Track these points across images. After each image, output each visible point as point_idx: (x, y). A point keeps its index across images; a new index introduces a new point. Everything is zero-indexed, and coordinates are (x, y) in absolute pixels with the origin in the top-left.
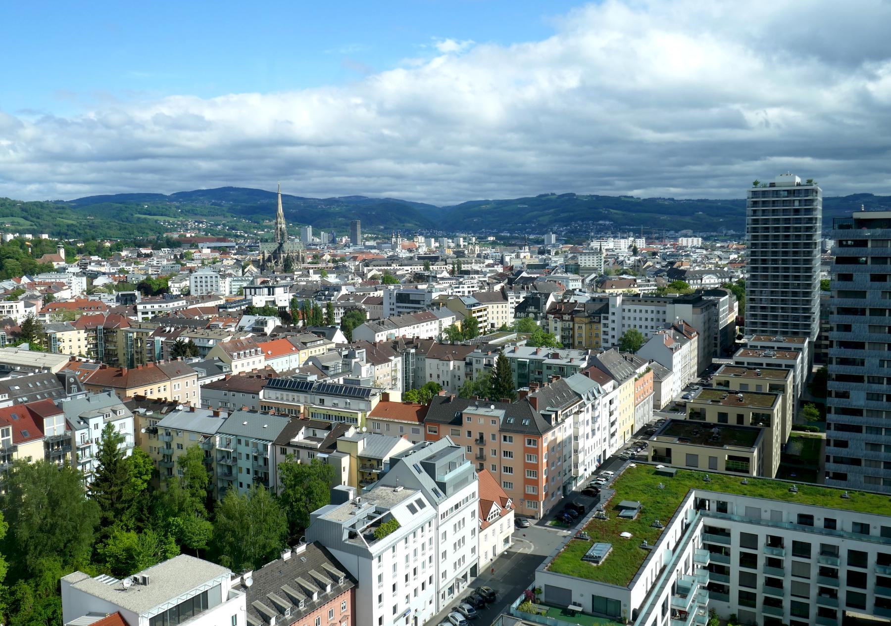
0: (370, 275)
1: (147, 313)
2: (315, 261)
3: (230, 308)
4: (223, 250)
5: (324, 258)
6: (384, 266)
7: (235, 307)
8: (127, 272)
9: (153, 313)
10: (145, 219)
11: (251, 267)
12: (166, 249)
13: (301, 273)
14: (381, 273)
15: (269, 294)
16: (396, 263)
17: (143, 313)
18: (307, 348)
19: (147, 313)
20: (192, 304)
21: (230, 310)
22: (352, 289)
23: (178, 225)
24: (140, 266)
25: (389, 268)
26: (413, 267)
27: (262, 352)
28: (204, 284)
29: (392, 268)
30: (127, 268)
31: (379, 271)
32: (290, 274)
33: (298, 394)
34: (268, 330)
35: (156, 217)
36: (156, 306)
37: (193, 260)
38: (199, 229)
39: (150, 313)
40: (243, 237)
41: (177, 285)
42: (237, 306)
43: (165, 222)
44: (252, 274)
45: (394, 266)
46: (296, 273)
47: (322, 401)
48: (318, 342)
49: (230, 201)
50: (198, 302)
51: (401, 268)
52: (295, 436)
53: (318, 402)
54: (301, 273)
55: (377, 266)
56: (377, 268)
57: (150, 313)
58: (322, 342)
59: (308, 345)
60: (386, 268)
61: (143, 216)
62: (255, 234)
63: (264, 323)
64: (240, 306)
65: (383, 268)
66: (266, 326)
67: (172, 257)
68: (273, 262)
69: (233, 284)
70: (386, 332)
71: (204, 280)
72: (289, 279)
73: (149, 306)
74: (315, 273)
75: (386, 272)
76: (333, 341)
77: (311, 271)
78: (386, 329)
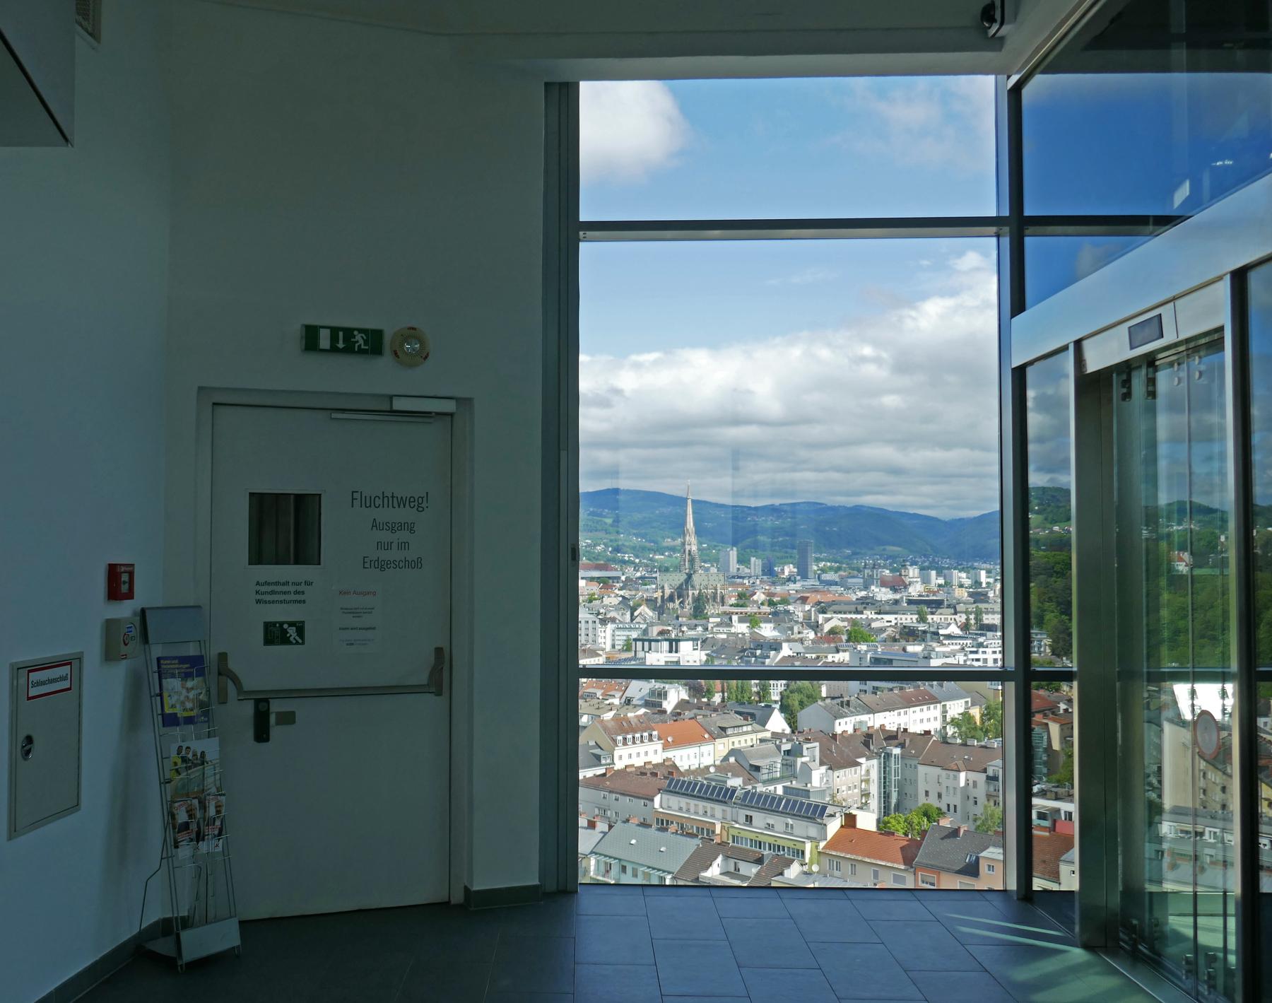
0: (827, 628)
2: (741, 602)
5: (755, 598)
6: (850, 613)
11: (644, 610)
13: (719, 620)
14: (846, 624)
15: (671, 651)
16: (871, 609)
18: (727, 736)
22: (799, 648)
25: (859, 616)
26: (899, 616)
27: (659, 739)
29: (864, 617)
31: (843, 620)
32: (703, 622)
33: (712, 805)
34: (669, 705)
40: (633, 563)
44: (645, 620)
45: (869, 614)
46: (711, 620)
47: (749, 819)
48: (745, 729)
51: (879, 617)
52: (707, 868)
53: (743, 819)
54: (719, 620)
55: (840, 612)
56: (840, 616)
58: (749, 728)
59: (729, 732)
60: (854, 616)
62: (651, 560)
63: (663, 695)
65: (849, 616)
66: (666, 699)
69: (617, 633)
70: (853, 719)
74: (741, 621)
75: (854, 623)
76: (767, 727)
77: (735, 618)
78: (853, 714)
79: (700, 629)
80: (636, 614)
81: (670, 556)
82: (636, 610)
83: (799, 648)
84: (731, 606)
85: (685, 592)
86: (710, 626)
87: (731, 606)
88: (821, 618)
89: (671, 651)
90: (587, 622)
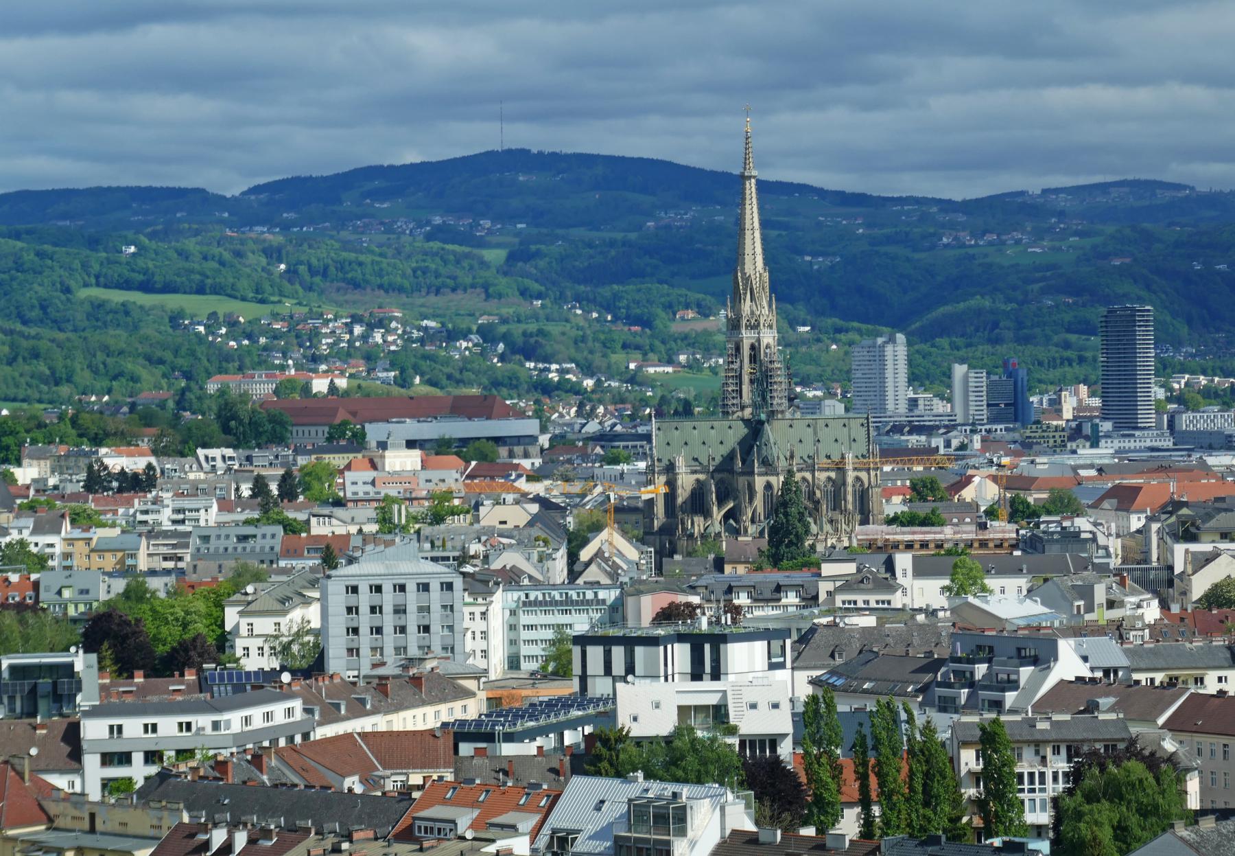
1: (124, 758)
2: (923, 509)
3: (510, 738)
4: (482, 457)
5: (968, 494)
7: (531, 735)
8: (41, 562)
9: (152, 757)
10: (125, 309)
12: (215, 452)
15: (696, 675)
17: (108, 759)
19: (124, 758)
20: (331, 716)
21: (508, 749)
23: (276, 336)
24: (98, 534)
28: (388, 621)
30: (39, 542)
35: (173, 301)
36: (168, 725)
37: (339, 503)
38: (370, 358)
39: (138, 758)
40: (576, 390)
41: (265, 625)
42: (543, 731)
43: (213, 321)
44: (614, 573)
46: (827, 569)
49: (514, 217)
50: (358, 710)
54: (851, 568)
57: (138, 758)
61: (117, 297)
62: (633, 379)
64: (559, 730)
67: (246, 491)
68: (717, 514)
69: (525, 619)
71: (388, 599)
72: (791, 599)
73: (133, 727)
74: (921, 570)
77: (903, 561)
79: (791, 599)
80: (585, 555)
81: (692, 366)
82: (585, 542)
83: (1111, 653)
84: (891, 521)
85: (742, 481)
86: (824, 588)
87: (891, 521)
88: (1180, 553)
89: (696, 675)
90: (425, 587)
